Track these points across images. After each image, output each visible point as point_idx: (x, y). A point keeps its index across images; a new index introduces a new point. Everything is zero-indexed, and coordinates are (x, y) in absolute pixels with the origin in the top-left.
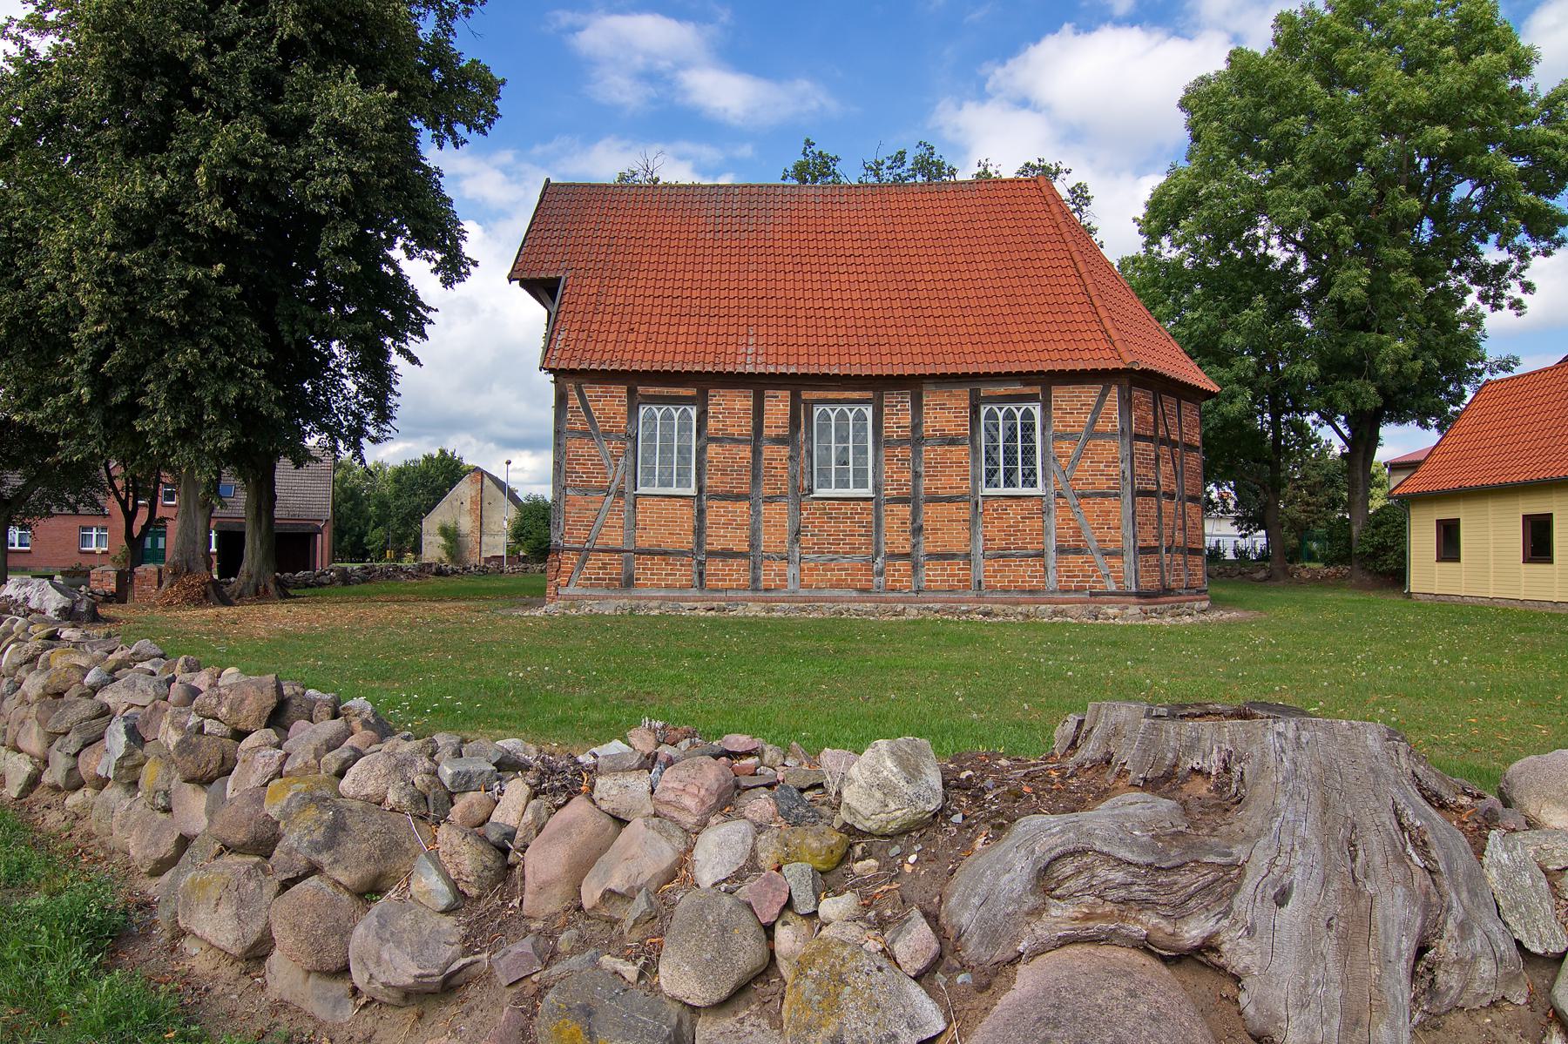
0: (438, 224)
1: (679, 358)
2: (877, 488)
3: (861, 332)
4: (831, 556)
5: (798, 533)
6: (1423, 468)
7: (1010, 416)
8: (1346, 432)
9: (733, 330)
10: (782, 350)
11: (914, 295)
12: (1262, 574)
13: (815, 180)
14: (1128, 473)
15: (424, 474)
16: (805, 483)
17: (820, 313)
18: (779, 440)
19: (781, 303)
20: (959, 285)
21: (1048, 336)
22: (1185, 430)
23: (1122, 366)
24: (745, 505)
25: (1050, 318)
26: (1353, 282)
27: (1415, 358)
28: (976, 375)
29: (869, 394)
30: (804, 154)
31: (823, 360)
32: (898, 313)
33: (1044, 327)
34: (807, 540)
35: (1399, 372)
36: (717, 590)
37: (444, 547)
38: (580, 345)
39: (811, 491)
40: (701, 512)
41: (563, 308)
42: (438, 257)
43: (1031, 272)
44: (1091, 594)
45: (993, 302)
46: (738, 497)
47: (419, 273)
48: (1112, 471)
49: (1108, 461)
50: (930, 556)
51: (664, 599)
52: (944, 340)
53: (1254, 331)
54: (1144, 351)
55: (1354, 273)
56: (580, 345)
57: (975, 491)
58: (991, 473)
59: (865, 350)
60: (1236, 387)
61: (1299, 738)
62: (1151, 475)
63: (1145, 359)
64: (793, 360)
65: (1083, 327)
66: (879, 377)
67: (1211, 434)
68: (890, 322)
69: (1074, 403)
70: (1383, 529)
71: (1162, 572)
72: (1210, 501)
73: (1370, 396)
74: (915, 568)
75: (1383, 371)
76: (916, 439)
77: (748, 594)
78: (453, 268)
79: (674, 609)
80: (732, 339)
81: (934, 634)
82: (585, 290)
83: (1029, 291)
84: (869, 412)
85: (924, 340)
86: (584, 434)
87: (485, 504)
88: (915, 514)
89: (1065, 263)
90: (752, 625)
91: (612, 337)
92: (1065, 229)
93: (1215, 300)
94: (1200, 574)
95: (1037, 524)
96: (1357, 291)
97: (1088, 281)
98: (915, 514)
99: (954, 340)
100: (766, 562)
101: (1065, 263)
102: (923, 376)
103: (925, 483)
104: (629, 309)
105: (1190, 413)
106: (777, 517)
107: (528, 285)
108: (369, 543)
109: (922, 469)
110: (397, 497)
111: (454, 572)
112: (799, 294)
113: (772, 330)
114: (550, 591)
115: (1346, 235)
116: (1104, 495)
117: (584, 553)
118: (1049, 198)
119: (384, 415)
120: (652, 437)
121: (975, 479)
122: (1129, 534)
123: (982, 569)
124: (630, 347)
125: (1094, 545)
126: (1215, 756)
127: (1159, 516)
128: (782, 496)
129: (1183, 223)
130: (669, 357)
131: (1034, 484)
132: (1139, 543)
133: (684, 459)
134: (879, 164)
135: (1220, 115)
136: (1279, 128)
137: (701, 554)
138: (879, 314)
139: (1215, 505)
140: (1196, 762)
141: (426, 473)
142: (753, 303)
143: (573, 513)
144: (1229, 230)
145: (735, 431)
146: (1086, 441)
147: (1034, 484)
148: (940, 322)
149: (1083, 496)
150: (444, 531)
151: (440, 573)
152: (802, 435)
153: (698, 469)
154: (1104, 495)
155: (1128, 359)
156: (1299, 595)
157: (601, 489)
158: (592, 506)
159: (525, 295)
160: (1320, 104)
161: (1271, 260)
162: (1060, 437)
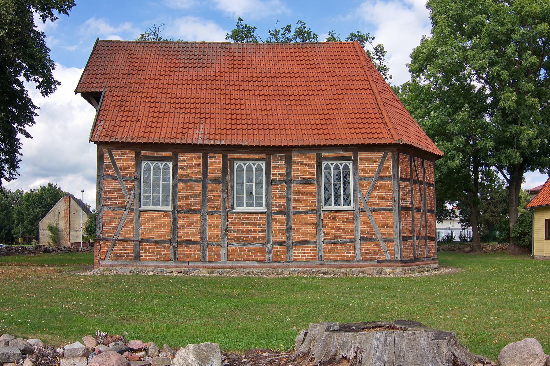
0: (40, 61)
1: (163, 136)
2: (268, 207)
3: (260, 122)
4: (244, 243)
5: (226, 231)
6: (540, 194)
7: (337, 168)
8: (508, 177)
9: (192, 120)
10: (218, 131)
11: (288, 103)
12: (469, 249)
13: (243, 39)
14: (397, 198)
15: (41, 197)
16: (230, 204)
17: (239, 112)
18: (216, 181)
19: (218, 106)
20: (312, 98)
21: (356, 126)
22: (426, 175)
23: (393, 142)
24: (198, 216)
25: (357, 116)
26: (509, 99)
27: (537, 138)
28: (319, 146)
29: (263, 156)
30: (238, 25)
31: (240, 137)
32: (279, 112)
33: (354, 121)
34: (231, 235)
35: (530, 145)
36: (184, 262)
37: (51, 237)
38: (111, 128)
39: (233, 208)
40: (175, 220)
41: (103, 108)
42: (40, 79)
43: (349, 92)
44: (378, 262)
45: (329, 107)
46: (195, 212)
47: (31, 89)
48: (389, 197)
49: (387, 192)
50: (296, 243)
51: (156, 266)
52: (303, 127)
53: (463, 122)
54: (405, 134)
55: (510, 94)
56: (111, 128)
57: (319, 208)
58: (327, 200)
59: (261, 132)
60: (455, 152)
61: (386, 341)
62: (409, 199)
63: (405, 138)
64: (223, 137)
65: (375, 121)
66: (269, 147)
67: (442, 177)
68: (275, 117)
69: (370, 161)
70: (524, 224)
71: (414, 250)
72: (448, 211)
73: (517, 158)
74: (288, 249)
75: (522, 144)
76: (288, 181)
77: (200, 264)
78: (48, 86)
79: (161, 272)
80: (191, 126)
81: (293, 284)
82: (115, 98)
83: (347, 101)
84: (263, 165)
85: (293, 127)
86: (113, 177)
87: (72, 214)
88: (288, 220)
89: (366, 87)
90: (200, 281)
91: (128, 124)
92: (366, 69)
93: (445, 107)
94: (434, 250)
95: (351, 225)
96: (511, 103)
97: (378, 97)
98: (288, 220)
99: (309, 127)
100: (209, 247)
101: (366, 87)
102: (291, 147)
103: (293, 204)
104: (137, 109)
105: (429, 166)
106: (215, 223)
107: (85, 95)
108: (15, 234)
109: (291, 196)
110: (27, 209)
111: (53, 251)
112: (228, 101)
113: (213, 121)
114: (96, 262)
115: (505, 74)
116: (385, 210)
117: (113, 241)
118: (359, 53)
119: (14, 166)
120: (148, 179)
121: (319, 202)
122: (397, 230)
123: (323, 249)
124: (137, 129)
125: (379, 236)
126: (352, 350)
127: (413, 220)
128: (218, 211)
129: (429, 67)
130: (157, 135)
131: (349, 204)
132: (402, 235)
133: (165, 191)
134: (277, 32)
135: (446, 12)
136: (473, 20)
137: (175, 242)
138: (270, 113)
139: (450, 213)
140: (343, 354)
141: (41, 196)
142: (204, 106)
143: (107, 220)
144: (453, 71)
145: (193, 176)
146: (376, 181)
147: (349, 204)
148: (301, 117)
149: (374, 210)
150: (51, 228)
151: (46, 251)
152: (228, 178)
153: (173, 196)
154: (385, 210)
155: (397, 138)
156: (483, 260)
157: (121, 207)
158: (117, 216)
159: (84, 100)
160: (492, 10)
161: (473, 87)
162: (363, 179)
